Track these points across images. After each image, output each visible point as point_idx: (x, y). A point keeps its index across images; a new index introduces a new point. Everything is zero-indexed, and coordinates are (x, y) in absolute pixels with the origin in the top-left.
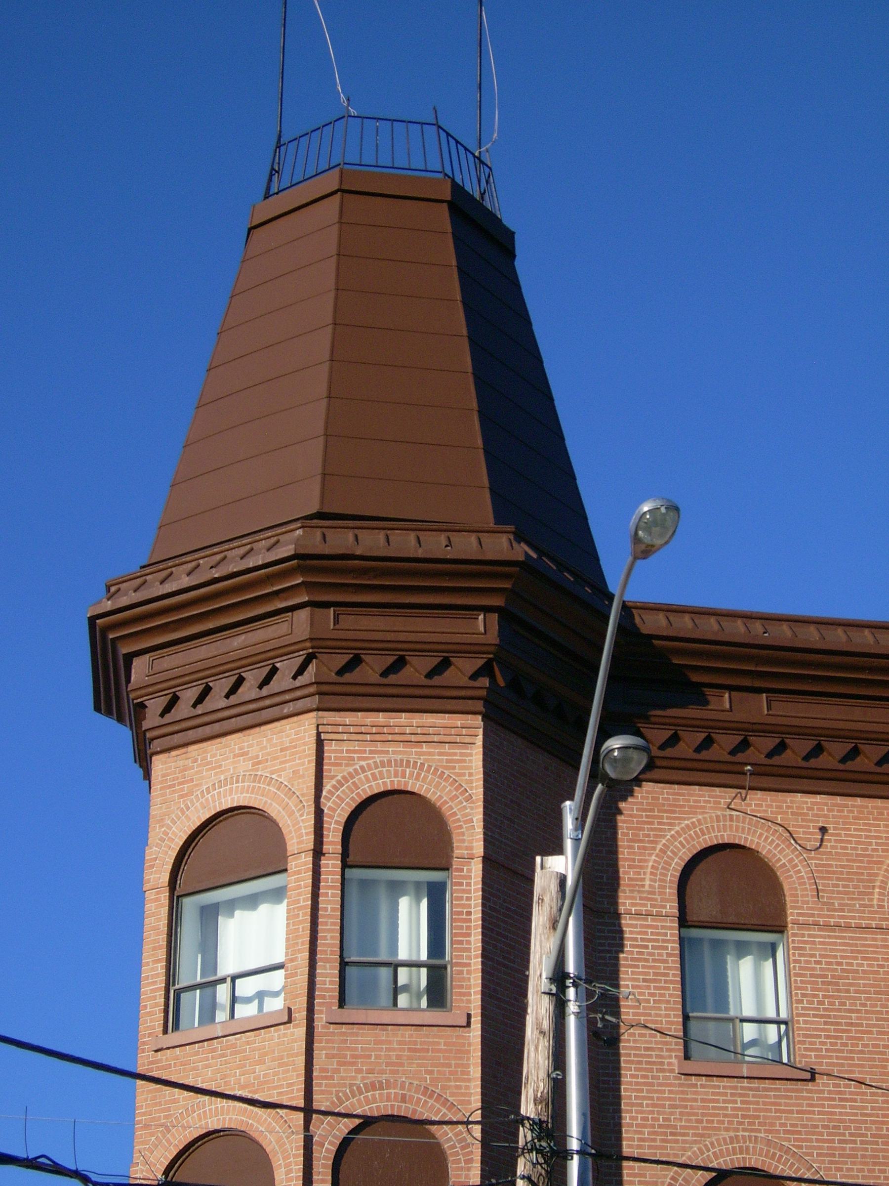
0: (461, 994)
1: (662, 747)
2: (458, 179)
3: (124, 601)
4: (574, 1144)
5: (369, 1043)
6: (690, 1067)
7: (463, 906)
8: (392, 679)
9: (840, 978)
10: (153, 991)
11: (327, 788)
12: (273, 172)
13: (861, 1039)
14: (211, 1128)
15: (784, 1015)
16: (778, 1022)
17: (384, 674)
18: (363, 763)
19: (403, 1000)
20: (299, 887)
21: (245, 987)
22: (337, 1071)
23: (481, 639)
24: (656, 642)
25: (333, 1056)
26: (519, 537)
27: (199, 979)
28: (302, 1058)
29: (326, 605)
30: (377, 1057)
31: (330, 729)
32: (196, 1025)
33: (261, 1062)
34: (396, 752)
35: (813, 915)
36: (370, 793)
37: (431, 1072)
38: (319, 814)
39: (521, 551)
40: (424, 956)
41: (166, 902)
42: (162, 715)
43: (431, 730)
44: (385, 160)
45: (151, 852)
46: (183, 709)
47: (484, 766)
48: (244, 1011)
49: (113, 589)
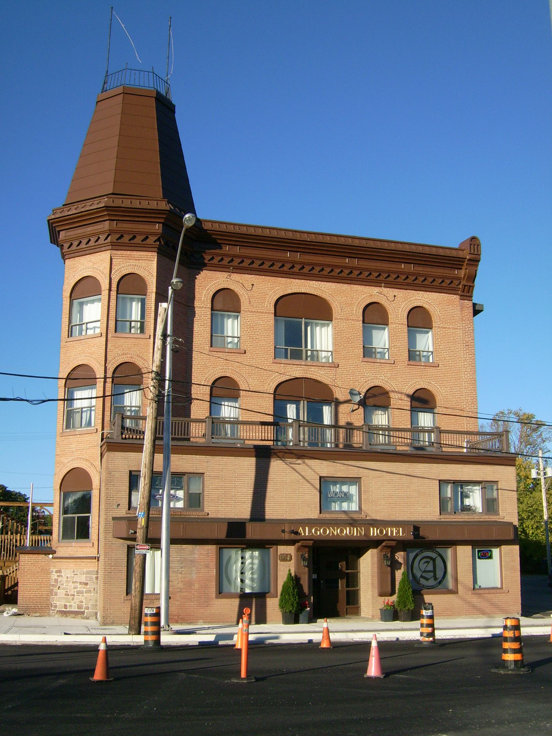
0: (148, 330)
1: (209, 261)
3: (57, 216)
4: (167, 378)
6: (212, 349)
7: (150, 306)
8: (132, 242)
9: (254, 326)
12: (105, 83)
13: (259, 343)
14: (80, 364)
15: (239, 336)
16: (238, 337)
17: (130, 240)
18: (123, 265)
19: (133, 331)
20: (105, 299)
21: (89, 326)
22: (114, 350)
25: (113, 346)
26: (169, 202)
27: (78, 323)
31: (114, 255)
32: (77, 335)
34: (132, 262)
35: (248, 308)
37: (139, 351)
38: (110, 279)
39: (169, 207)
40: (139, 319)
41: (69, 301)
42: (68, 248)
43: (142, 256)
45: (65, 287)
46: (74, 247)
47: (157, 267)
48: (90, 332)
49: (54, 212)
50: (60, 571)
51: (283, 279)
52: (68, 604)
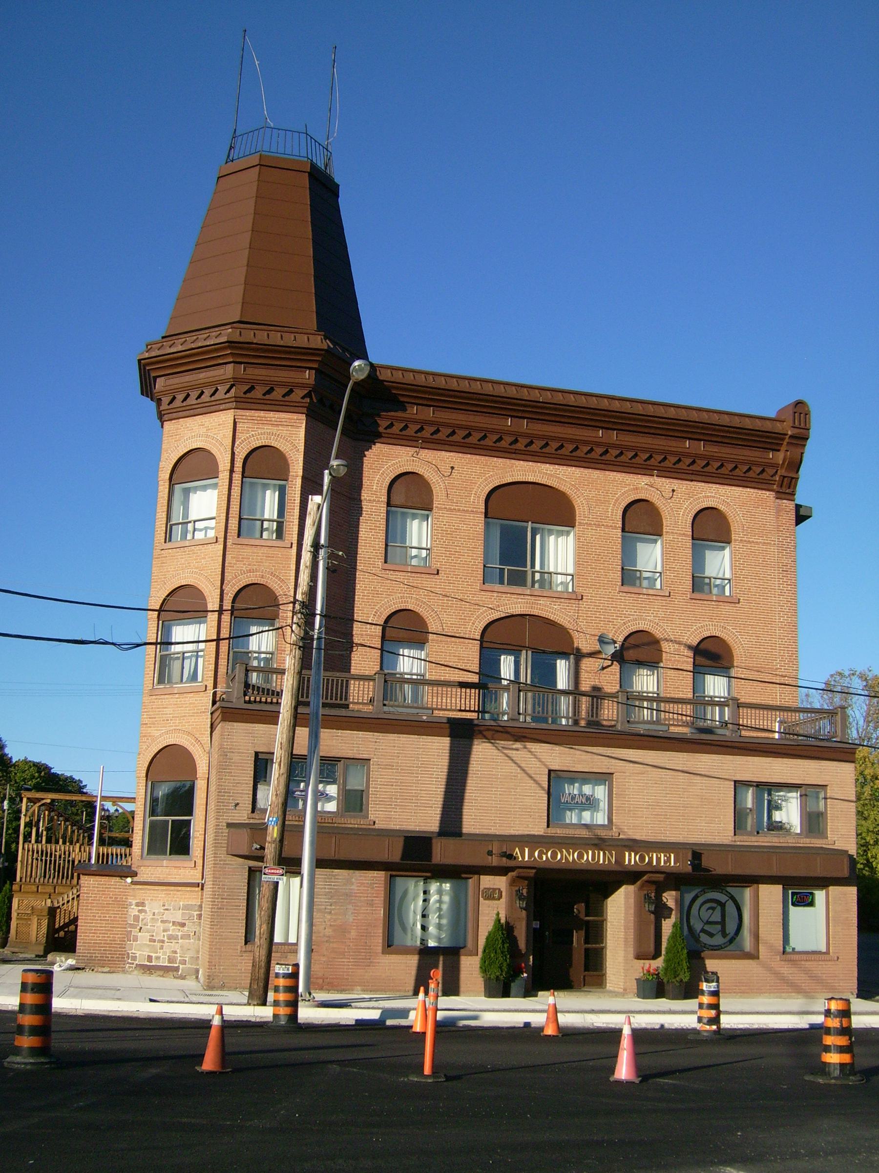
2: (314, 161)
3: (153, 354)
5: (249, 553)
6: (387, 566)
8: (267, 397)
10: (161, 524)
11: (237, 443)
15: (429, 546)
16: (427, 549)
21: (199, 525)
23: (307, 382)
24: (385, 383)
25: (234, 558)
27: (181, 521)
28: (221, 558)
29: (240, 363)
30: (253, 559)
31: (240, 417)
33: (204, 558)
34: (268, 429)
36: (255, 446)
37: (273, 566)
38: (233, 454)
39: (326, 344)
40: (275, 517)
41: (168, 486)
42: (169, 405)
43: (283, 420)
44: (281, 150)
45: (162, 464)
46: (178, 403)
47: (305, 437)
48: (199, 535)
49: (149, 347)
50: (142, 904)
51: (500, 460)
52: (154, 955)
